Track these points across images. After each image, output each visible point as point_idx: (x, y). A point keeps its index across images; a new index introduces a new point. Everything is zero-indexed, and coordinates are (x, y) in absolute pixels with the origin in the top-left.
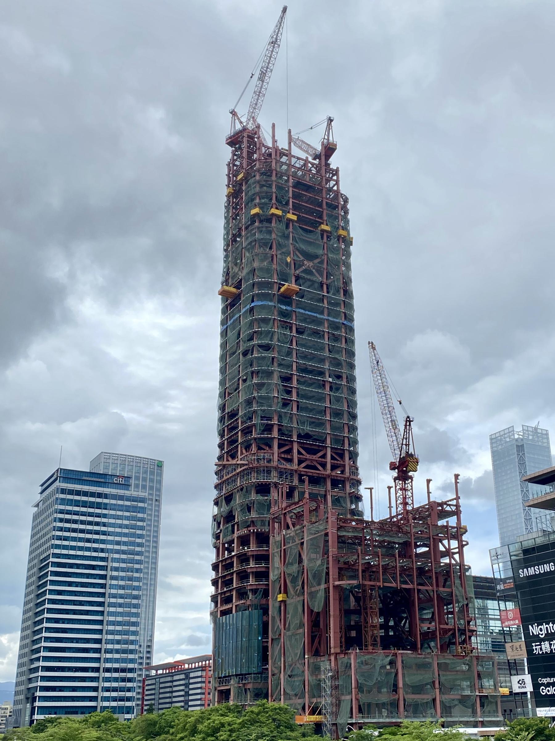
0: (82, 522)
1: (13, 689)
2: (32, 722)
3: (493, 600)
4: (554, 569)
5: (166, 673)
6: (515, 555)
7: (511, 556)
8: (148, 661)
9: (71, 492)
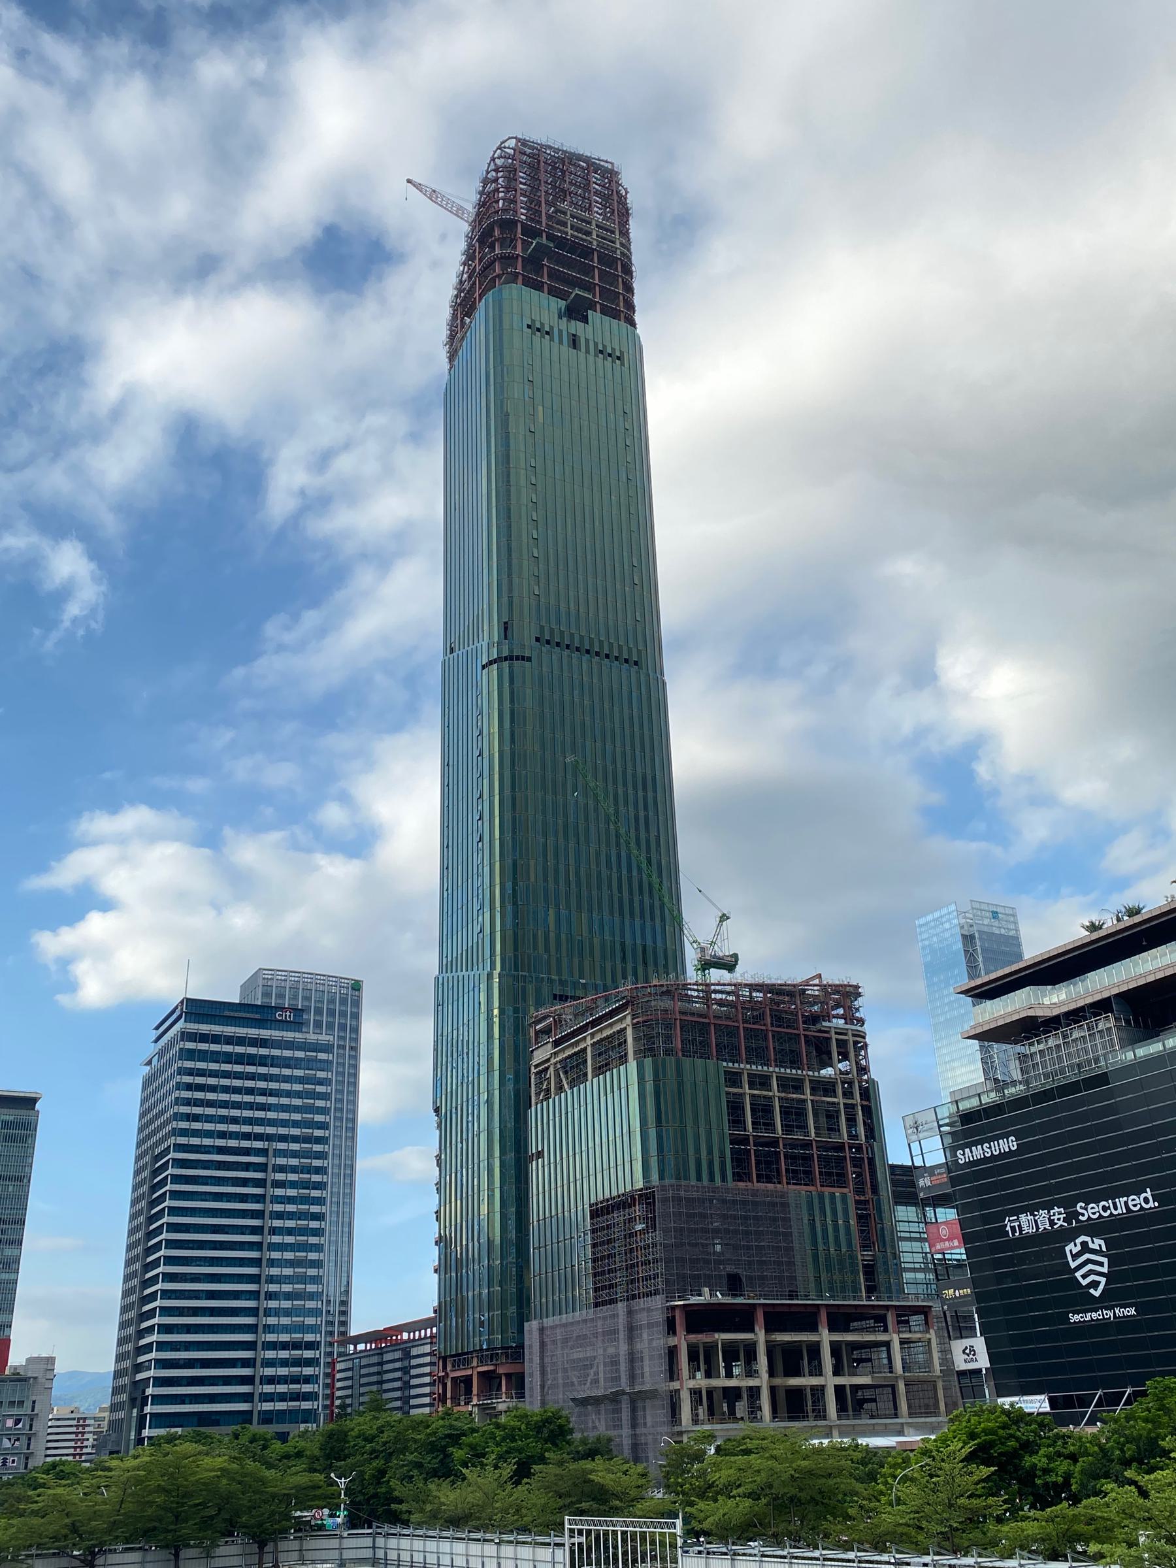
0: (226, 1089)
1: (109, 1383)
2: (140, 1441)
3: (906, 1204)
4: (1016, 1147)
5: (371, 1349)
6: (946, 1125)
7: (940, 1126)
8: (342, 1329)
9: (204, 1038)
